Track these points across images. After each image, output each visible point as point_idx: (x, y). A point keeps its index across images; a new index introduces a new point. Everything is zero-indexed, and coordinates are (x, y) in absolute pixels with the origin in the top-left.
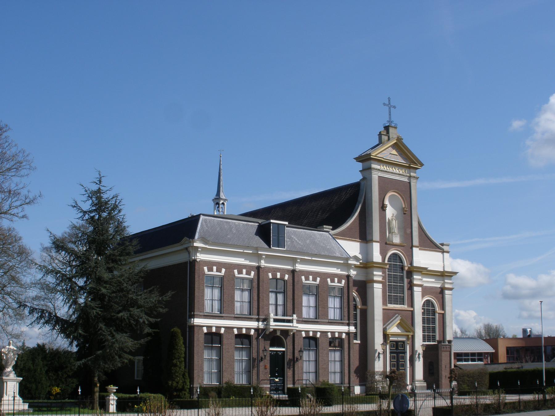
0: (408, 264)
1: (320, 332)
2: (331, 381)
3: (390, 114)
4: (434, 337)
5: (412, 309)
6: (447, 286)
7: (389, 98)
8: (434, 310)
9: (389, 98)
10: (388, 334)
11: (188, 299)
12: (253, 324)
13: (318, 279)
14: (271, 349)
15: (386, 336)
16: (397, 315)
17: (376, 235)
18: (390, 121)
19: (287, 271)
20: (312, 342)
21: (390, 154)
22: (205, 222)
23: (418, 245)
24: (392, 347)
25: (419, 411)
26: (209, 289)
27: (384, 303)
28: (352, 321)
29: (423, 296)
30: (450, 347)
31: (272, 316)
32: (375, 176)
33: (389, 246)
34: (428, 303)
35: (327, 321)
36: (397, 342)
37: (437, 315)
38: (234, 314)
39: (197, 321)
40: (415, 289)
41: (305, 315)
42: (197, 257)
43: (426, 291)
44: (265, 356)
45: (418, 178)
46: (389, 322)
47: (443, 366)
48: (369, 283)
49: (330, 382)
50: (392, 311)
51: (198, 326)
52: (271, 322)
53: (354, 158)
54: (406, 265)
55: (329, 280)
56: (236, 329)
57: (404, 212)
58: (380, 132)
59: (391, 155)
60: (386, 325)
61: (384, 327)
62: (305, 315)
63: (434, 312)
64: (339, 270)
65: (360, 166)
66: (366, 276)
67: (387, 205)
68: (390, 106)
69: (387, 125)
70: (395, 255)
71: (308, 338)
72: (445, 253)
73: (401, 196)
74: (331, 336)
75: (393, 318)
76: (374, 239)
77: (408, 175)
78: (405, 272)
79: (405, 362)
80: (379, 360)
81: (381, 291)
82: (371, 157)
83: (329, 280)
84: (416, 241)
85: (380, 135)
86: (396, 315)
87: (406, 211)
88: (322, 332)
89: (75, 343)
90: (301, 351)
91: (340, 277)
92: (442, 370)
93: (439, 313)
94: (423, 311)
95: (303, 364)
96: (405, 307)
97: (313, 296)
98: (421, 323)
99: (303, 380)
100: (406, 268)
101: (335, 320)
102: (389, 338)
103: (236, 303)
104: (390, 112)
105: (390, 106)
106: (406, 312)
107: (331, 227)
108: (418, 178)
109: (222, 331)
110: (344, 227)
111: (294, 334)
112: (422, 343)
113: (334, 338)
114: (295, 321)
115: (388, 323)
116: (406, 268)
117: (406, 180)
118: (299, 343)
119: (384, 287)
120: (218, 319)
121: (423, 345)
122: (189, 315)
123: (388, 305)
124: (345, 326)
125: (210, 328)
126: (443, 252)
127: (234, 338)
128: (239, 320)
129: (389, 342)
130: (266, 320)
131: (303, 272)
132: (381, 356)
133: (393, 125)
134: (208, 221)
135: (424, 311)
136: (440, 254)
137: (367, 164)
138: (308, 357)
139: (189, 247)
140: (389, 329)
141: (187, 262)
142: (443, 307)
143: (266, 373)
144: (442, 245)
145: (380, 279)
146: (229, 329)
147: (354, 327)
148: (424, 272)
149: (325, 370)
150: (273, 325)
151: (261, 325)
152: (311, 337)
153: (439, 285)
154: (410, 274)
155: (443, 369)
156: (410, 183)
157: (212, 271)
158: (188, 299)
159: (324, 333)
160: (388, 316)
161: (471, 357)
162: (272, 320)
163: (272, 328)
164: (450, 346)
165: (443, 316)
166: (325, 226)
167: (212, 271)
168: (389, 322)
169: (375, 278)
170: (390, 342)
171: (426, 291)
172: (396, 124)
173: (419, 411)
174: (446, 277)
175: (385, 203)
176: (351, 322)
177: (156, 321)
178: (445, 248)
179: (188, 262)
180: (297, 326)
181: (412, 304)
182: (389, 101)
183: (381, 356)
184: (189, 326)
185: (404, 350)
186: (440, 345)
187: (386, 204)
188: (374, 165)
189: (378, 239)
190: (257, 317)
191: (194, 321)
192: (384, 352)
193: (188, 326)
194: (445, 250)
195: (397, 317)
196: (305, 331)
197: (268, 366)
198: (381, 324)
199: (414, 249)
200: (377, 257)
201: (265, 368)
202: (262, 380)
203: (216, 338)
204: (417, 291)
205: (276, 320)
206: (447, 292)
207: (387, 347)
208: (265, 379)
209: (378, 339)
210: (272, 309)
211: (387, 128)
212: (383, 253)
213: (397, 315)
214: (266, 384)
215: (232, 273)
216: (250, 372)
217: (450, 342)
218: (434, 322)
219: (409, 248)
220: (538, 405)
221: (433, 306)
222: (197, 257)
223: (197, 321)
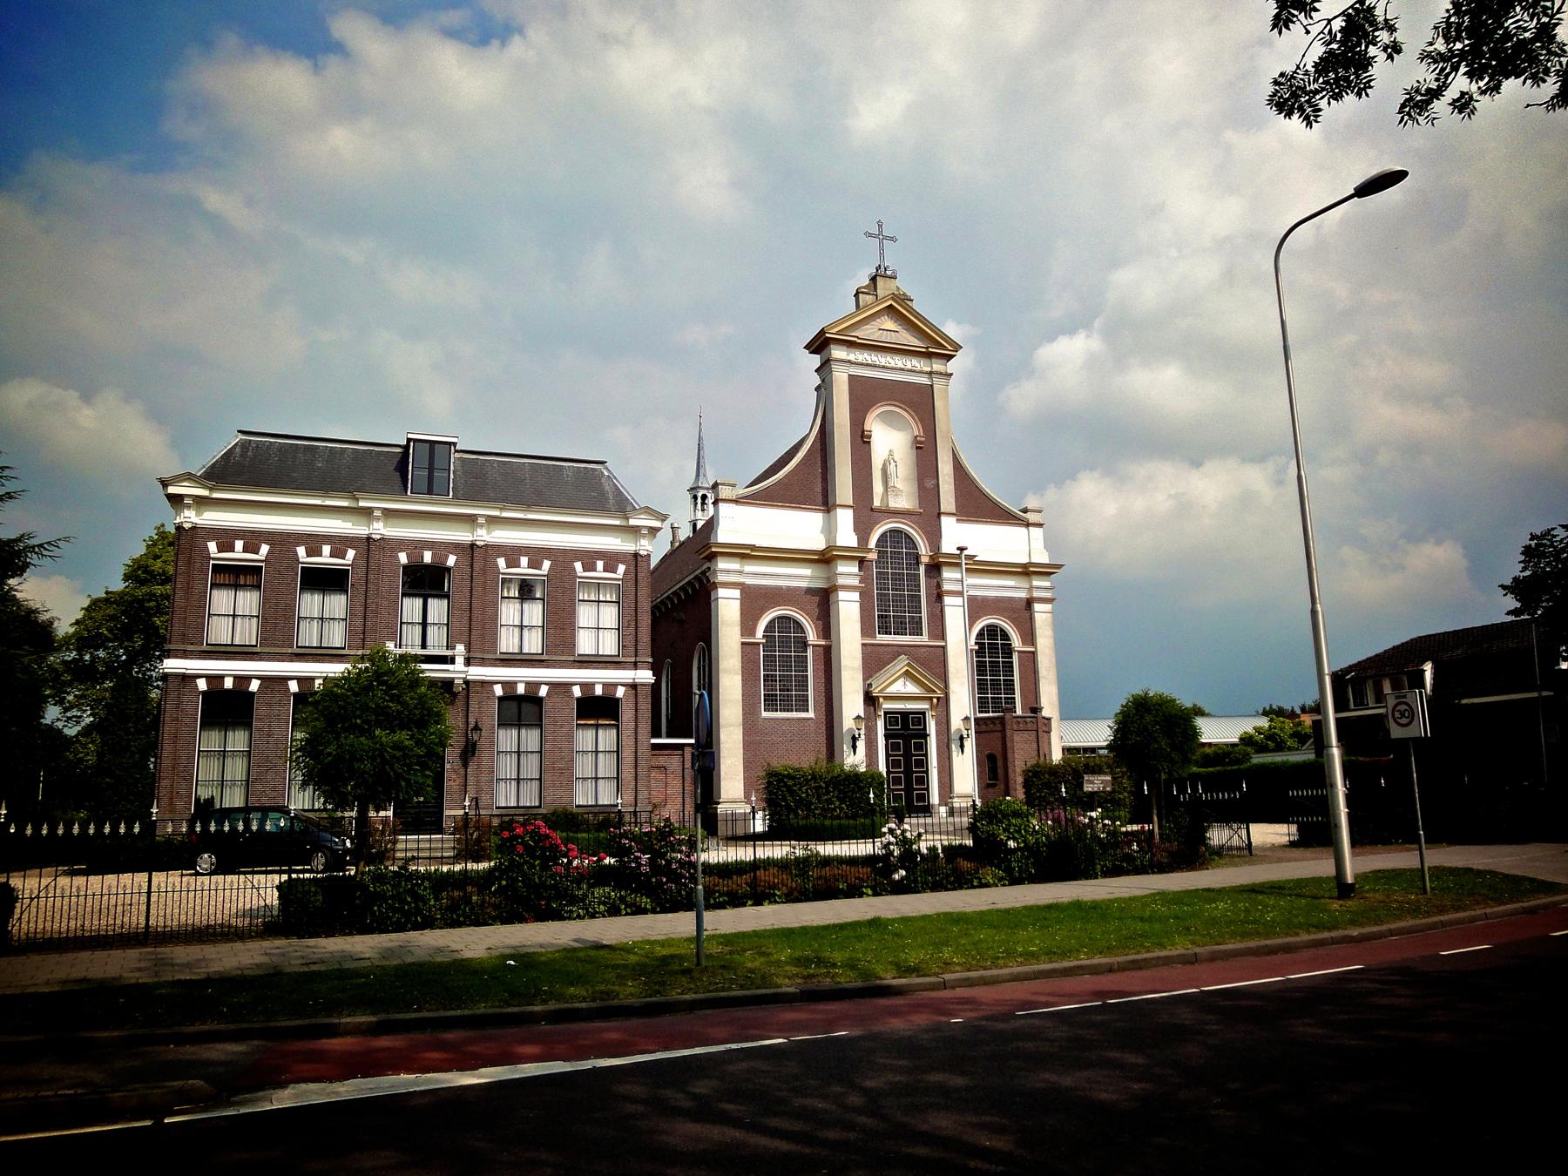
1: (258, 678)
5: (1033, 650)
6: (1036, 594)
10: (878, 697)
15: (870, 700)
19: (456, 547)
21: (880, 329)
23: (954, 512)
24: (916, 725)
26: (316, 596)
27: (866, 630)
33: (880, 514)
36: (905, 715)
40: (947, 600)
43: (977, 607)
45: (951, 374)
48: (832, 592)
50: (890, 649)
54: (924, 553)
56: (295, 681)
63: (1008, 650)
64: (620, 540)
65: (816, 360)
66: (828, 578)
72: (1030, 528)
73: (901, 408)
77: (929, 369)
78: (922, 569)
79: (926, 755)
80: (855, 754)
82: (827, 335)
84: (948, 500)
87: (921, 442)
88: (554, 686)
89: (92, 719)
91: (611, 560)
93: (1019, 652)
96: (924, 639)
97: (592, 606)
100: (925, 560)
101: (598, 655)
105: (880, 236)
108: (951, 374)
114: (460, 660)
116: (925, 560)
117: (925, 380)
125: (215, 681)
126: (1028, 525)
131: (500, 550)
132: (861, 745)
136: (1023, 530)
144: (1025, 511)
145: (855, 582)
146: (273, 683)
147: (651, 672)
152: (521, 696)
153: (1023, 595)
154: (935, 568)
156: (932, 386)
160: (874, 661)
169: (841, 581)
171: (977, 607)
174: (1034, 577)
181: (939, 630)
182: (880, 226)
185: (925, 728)
188: (836, 352)
196: (581, 685)
199: (944, 519)
200: (846, 536)
203: (527, 708)
206: (1037, 607)
209: (852, 705)
212: (862, 529)
215: (291, 554)
219: (929, 517)
220: (650, 970)
221: (1005, 636)
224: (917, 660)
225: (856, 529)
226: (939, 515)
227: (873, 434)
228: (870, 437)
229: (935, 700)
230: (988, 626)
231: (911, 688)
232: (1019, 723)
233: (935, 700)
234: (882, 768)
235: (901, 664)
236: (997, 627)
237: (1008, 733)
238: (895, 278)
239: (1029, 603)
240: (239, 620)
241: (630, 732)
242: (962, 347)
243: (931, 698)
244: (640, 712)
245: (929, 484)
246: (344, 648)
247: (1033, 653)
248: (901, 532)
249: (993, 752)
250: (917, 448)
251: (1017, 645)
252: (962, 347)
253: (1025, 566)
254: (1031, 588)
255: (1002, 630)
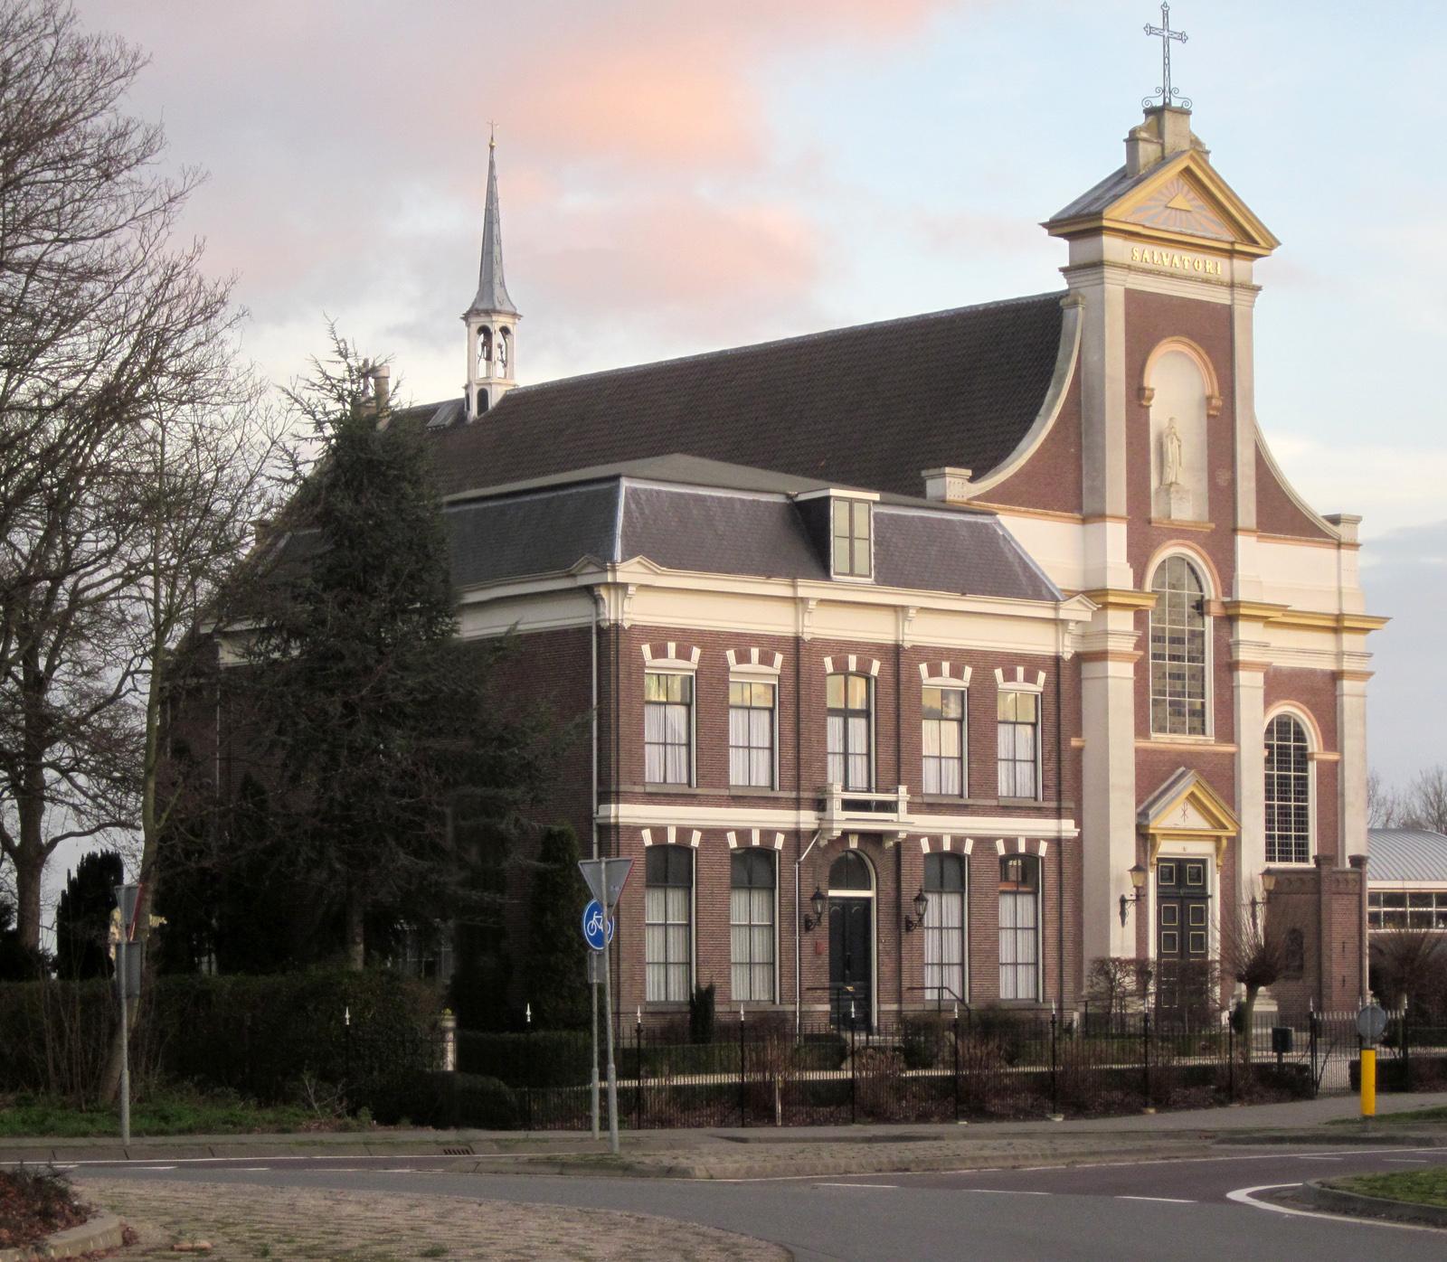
0: (1220, 595)
2: (1006, 993)
3: (1167, 65)
4: (1302, 843)
6: (1348, 665)
7: (1165, 5)
8: (1304, 748)
9: (1165, 5)
11: (595, 742)
12: (783, 819)
13: (968, 671)
14: (832, 893)
15: (1144, 837)
16: (1182, 769)
17: (1116, 494)
18: (1166, 91)
20: (951, 868)
21: (1167, 207)
22: (638, 503)
25: (1322, 1069)
27: (1141, 730)
28: (1066, 804)
29: (1268, 703)
30: (1361, 881)
31: (838, 794)
32: (1115, 287)
34: (1282, 728)
35: (994, 803)
36: (1181, 863)
37: (1312, 768)
38: (727, 786)
39: (626, 813)
40: (1243, 677)
41: (930, 786)
42: (625, 616)
44: (820, 915)
45: (1259, 288)
46: (1156, 793)
47: (1336, 946)
49: (1002, 996)
51: (628, 827)
52: (835, 811)
53: (1045, 225)
55: (999, 673)
57: (1208, 409)
58: (1133, 133)
59: (1169, 211)
60: (1146, 803)
61: (1139, 810)
62: (930, 786)
63: (1303, 758)
65: (1060, 251)
67: (1152, 390)
68: (1166, 33)
69: (1158, 103)
70: (1180, 559)
71: (938, 856)
74: (1006, 850)
75: (1167, 778)
76: (1108, 512)
78: (1209, 621)
81: (1129, 686)
83: (999, 673)
85: (1132, 140)
86: (1178, 768)
90: (920, 899)
92: (1330, 958)
94: (1266, 753)
95: (922, 938)
96: (1207, 741)
98: (1263, 795)
99: (923, 988)
102: (1154, 846)
103: (732, 752)
104: (1166, 57)
105: (1166, 33)
106: (656, 475)
107: (969, 473)
108: (1259, 288)
109: (696, 840)
110: (1011, 467)
111: (898, 845)
112: (1264, 865)
113: (1012, 853)
114: (902, 807)
115: (1151, 798)
117: (1220, 297)
118: (913, 877)
119: (1140, 668)
120: (682, 805)
121: (1268, 872)
122: (599, 794)
123: (1154, 735)
124: (1046, 817)
127: (727, 861)
128: (744, 807)
129: (1155, 861)
130: (820, 805)
132: (1131, 910)
133: (1176, 103)
134: (643, 497)
135: (1271, 754)
136: (1329, 553)
137: (1087, 248)
138: (942, 910)
139: (599, 585)
140: (1156, 815)
141: (590, 628)
142: (1332, 737)
143: (819, 967)
144: (1335, 520)
146: (714, 835)
148: (1277, 618)
149: (988, 957)
150: (841, 819)
151: (808, 819)
153: (1328, 665)
154: (1229, 618)
155: (1334, 956)
157: (665, 655)
158: (595, 742)
159: (984, 843)
161: (1430, 913)
162: (836, 805)
163: (838, 829)
164: (1361, 874)
165: (1332, 774)
166: (948, 470)
167: (665, 655)
168: (1156, 793)
170: (1159, 860)
171: (1278, 684)
172: (1187, 100)
173: (1322, 1069)
175: (1146, 385)
176: (1065, 804)
177: (1400, 934)
178: (1342, 531)
179: (594, 631)
180: (904, 822)
181: (1228, 730)
182: (1166, 15)
183: (1131, 910)
184: (599, 826)
185: (1204, 887)
186: (1325, 870)
187: (1151, 386)
189: (1123, 511)
190: (793, 795)
191: (617, 809)
192: (1140, 897)
193: (595, 828)
194: (1343, 540)
195: (1182, 775)
197: (825, 945)
198: (1131, 800)
200: (1119, 575)
201: (817, 953)
202: (808, 989)
203: (760, 869)
204: (1249, 685)
205: (849, 805)
207: (1146, 878)
208: (816, 985)
210: (834, 767)
211: (1155, 113)
212: (1138, 557)
213: (1182, 769)
214: (819, 1001)
216: (774, 964)
217: (1358, 861)
218: (1302, 792)
221: (1300, 736)
222: (625, 616)
223: (626, 813)
224: (1201, 775)
225: (1132, 558)
226: (1235, 530)
227: (1155, 392)
228: (1150, 399)
229: (1224, 842)
230: (1279, 717)
231: (1196, 821)
232: (1338, 881)
233: (1224, 842)
234: (1152, 953)
235: (1188, 785)
236: (1289, 717)
237: (1325, 898)
238: (1188, 113)
239: (1336, 676)
240: (669, 748)
241: (1051, 903)
242: (1279, 244)
243: (1218, 839)
244: (1065, 876)
245: (1223, 479)
246: (846, 788)
247: (1232, 755)
248: (1184, 560)
249: (1298, 926)
250: (1209, 416)
251: (1316, 750)
252: (1279, 244)
253: (1339, 617)
254: (1340, 655)
255: (1297, 725)
